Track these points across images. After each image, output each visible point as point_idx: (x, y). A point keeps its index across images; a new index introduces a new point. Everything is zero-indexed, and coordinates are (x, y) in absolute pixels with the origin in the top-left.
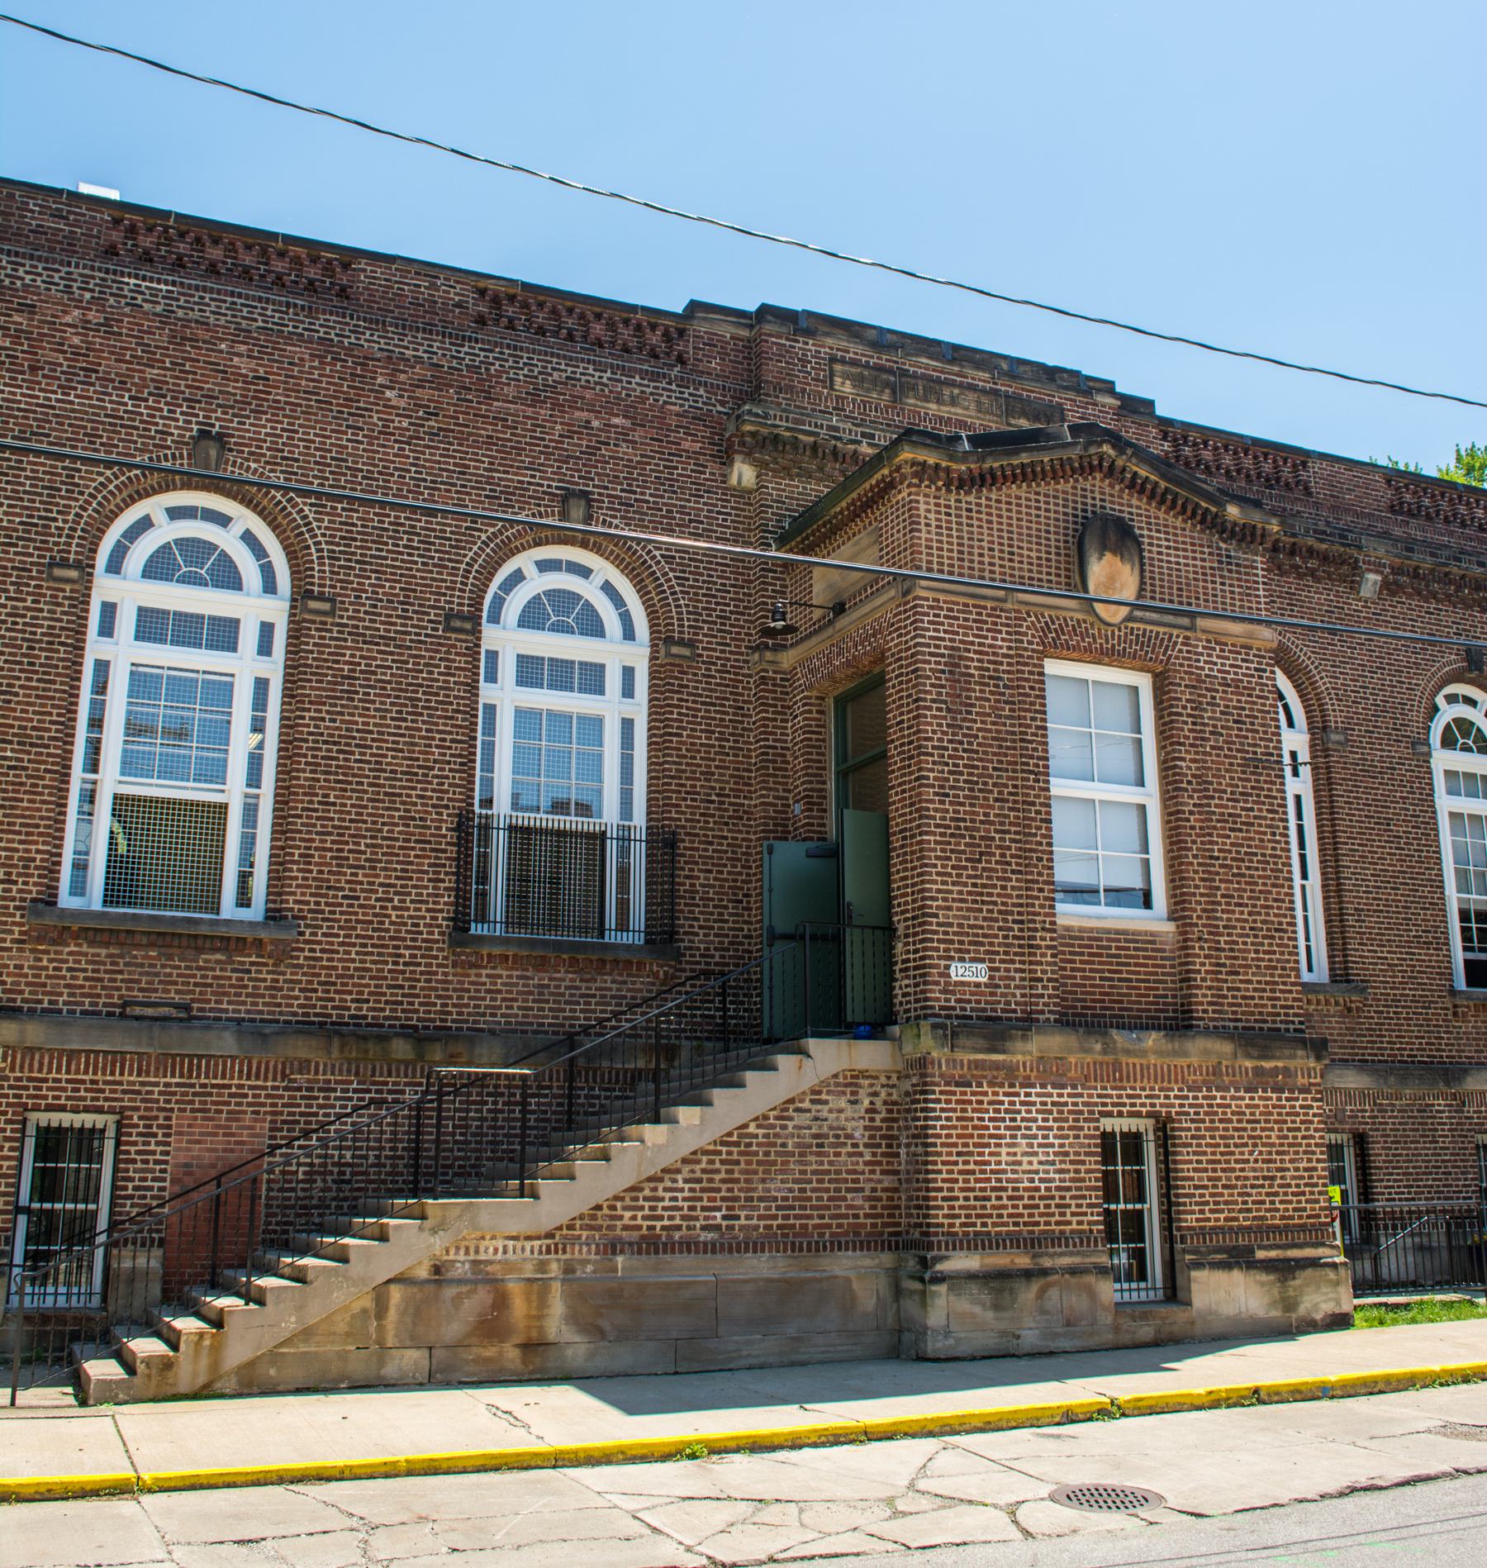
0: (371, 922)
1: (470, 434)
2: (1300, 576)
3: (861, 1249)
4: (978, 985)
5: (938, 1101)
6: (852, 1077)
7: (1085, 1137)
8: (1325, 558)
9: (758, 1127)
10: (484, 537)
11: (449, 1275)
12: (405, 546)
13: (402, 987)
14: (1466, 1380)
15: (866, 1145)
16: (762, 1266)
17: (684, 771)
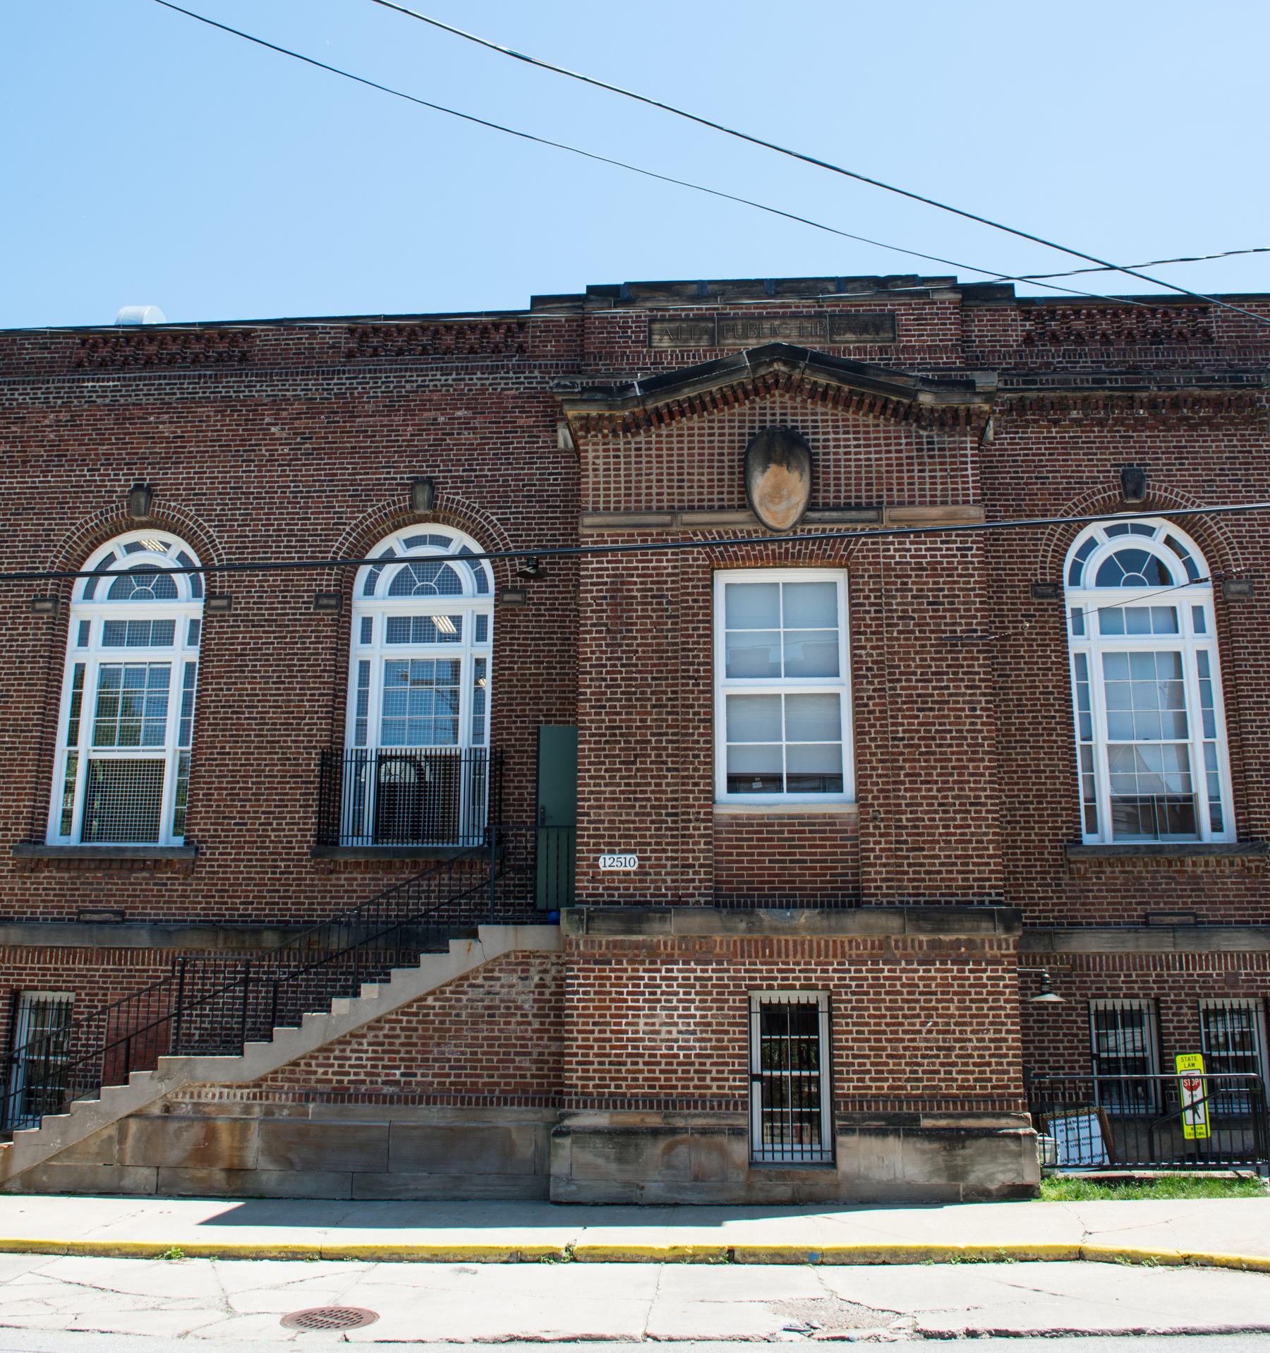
0: (255, 842)
1: (337, 448)
2: (1193, 428)
3: (526, 1105)
4: (627, 873)
5: (577, 977)
6: (523, 957)
7: (730, 1008)
8: (1217, 404)
9: (435, 1000)
10: (348, 529)
11: (176, 1113)
12: (286, 547)
13: (278, 891)
14: (999, 1259)
15: (535, 1016)
16: (433, 1116)
17: (516, 698)
